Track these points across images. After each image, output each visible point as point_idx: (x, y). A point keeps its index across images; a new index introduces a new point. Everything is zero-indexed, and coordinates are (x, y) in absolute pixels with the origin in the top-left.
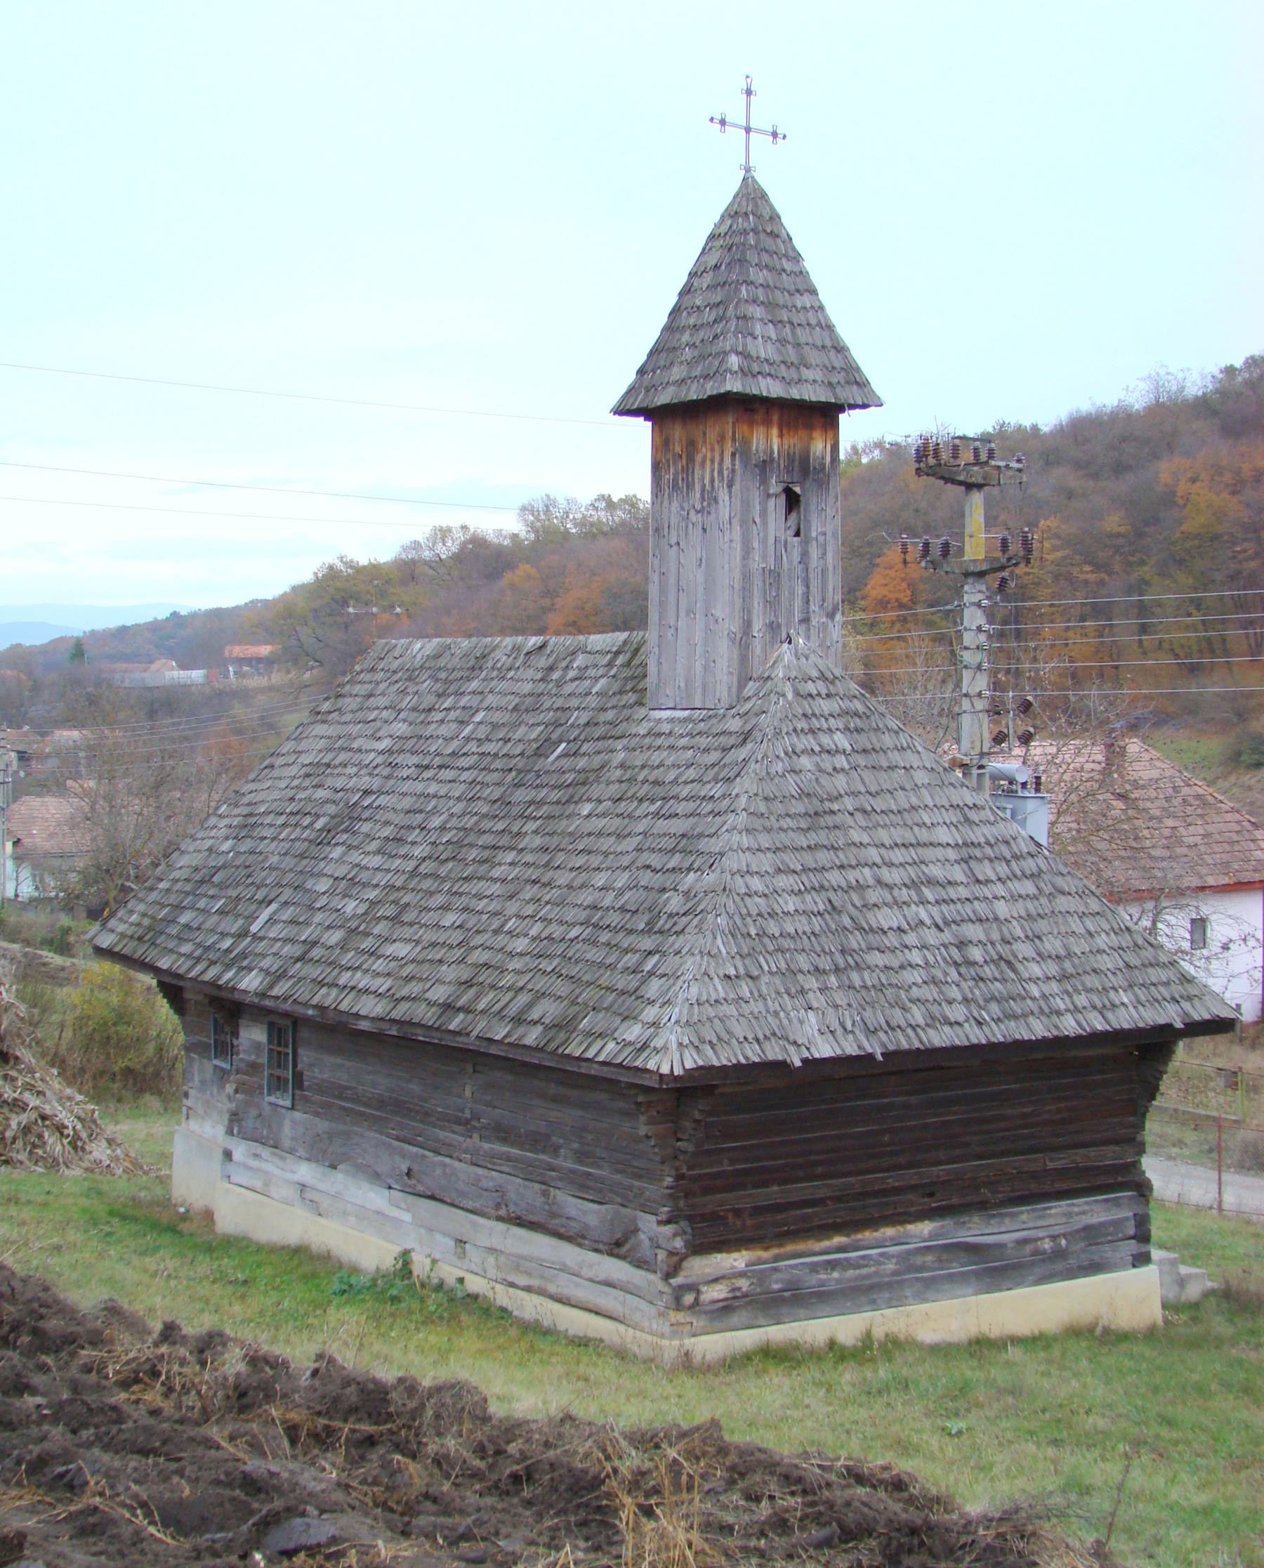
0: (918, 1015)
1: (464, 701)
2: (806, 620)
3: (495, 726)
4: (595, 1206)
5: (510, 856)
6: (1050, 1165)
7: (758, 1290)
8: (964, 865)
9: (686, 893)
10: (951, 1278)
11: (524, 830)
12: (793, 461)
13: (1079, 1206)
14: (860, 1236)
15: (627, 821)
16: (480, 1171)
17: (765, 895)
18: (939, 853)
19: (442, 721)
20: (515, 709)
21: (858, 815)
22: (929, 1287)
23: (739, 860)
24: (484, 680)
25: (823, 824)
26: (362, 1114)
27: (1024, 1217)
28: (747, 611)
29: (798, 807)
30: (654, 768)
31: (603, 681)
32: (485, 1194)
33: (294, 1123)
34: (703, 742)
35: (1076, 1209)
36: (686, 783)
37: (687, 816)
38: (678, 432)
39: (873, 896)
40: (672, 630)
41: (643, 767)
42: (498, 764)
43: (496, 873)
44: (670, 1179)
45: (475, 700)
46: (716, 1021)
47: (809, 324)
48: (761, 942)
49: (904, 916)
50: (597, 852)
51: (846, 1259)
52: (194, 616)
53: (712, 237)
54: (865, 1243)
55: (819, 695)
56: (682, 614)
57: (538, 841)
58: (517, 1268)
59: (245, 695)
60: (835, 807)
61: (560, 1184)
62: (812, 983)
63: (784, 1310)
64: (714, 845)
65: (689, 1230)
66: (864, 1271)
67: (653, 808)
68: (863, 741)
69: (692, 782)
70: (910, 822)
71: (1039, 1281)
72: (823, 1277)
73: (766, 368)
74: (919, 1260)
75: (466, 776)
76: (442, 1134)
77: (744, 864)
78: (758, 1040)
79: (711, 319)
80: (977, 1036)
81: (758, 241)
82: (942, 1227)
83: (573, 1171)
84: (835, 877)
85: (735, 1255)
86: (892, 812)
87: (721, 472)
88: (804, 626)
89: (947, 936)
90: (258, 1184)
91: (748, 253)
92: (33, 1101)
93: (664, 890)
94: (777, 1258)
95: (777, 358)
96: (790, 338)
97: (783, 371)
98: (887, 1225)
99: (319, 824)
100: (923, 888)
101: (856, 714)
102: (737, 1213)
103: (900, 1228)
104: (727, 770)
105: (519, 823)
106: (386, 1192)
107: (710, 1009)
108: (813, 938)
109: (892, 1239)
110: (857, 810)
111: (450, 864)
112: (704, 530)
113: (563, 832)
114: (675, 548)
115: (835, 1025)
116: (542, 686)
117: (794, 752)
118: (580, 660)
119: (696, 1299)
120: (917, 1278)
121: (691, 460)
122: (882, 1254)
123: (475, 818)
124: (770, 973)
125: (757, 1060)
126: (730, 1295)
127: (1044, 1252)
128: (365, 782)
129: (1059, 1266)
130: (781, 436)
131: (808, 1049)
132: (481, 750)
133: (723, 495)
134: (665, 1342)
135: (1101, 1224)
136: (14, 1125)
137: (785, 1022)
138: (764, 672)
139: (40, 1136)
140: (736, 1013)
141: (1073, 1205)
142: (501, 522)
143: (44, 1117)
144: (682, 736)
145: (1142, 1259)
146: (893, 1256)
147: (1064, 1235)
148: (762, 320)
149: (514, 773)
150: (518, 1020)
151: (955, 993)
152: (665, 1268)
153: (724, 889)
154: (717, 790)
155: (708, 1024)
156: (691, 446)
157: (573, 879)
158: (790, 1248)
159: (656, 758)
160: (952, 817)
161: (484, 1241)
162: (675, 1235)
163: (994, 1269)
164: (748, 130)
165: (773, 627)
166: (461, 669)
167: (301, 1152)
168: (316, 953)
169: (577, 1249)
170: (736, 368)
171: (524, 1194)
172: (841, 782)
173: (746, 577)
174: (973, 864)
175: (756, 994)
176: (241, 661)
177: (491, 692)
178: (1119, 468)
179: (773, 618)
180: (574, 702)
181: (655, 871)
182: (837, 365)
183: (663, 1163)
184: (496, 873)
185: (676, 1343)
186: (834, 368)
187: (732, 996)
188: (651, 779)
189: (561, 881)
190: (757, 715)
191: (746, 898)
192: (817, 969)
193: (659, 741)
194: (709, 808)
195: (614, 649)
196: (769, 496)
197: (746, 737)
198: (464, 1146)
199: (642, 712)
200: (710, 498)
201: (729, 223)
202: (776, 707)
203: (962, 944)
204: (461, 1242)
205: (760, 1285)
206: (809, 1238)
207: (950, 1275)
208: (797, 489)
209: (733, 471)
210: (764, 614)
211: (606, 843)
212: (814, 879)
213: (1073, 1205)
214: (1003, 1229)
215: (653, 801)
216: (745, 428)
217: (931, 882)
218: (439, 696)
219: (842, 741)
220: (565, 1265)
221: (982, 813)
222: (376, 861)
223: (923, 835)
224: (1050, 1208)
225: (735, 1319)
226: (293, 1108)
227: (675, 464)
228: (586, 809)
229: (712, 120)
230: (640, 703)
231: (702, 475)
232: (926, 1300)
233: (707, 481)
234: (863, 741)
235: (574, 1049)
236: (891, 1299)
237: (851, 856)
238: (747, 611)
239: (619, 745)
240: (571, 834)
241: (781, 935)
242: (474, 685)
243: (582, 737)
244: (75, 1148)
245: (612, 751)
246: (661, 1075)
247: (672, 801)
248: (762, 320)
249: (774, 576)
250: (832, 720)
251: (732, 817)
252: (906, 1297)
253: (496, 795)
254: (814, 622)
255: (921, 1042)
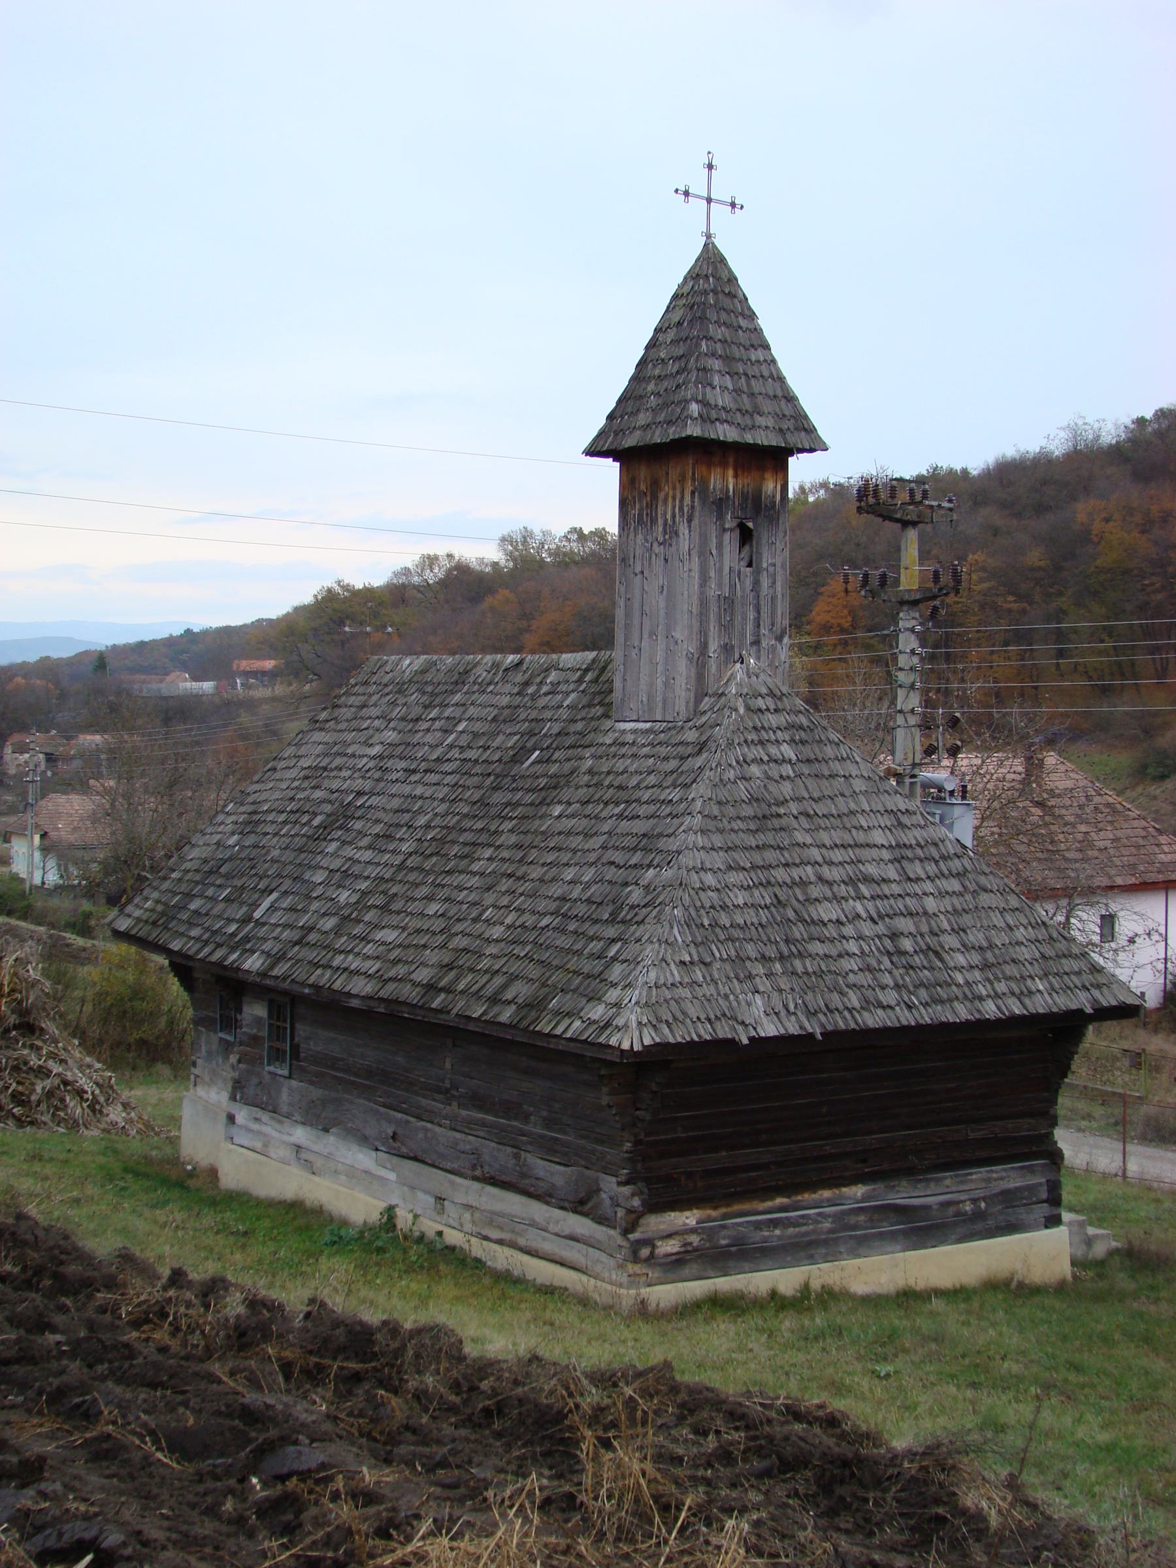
0: (854, 1000)
1: (448, 712)
2: (756, 643)
3: (476, 735)
4: (562, 1168)
5: (488, 852)
6: (972, 1136)
7: (708, 1245)
8: (897, 865)
9: (647, 887)
10: (881, 1236)
11: (500, 829)
12: (747, 499)
13: (996, 1172)
14: (799, 1198)
15: (593, 821)
16: (458, 1135)
17: (718, 890)
18: (875, 853)
19: (428, 730)
20: (494, 719)
21: (802, 819)
22: (862, 1244)
23: (694, 858)
24: (466, 693)
25: (770, 826)
26: (353, 1083)
27: (948, 1182)
28: (703, 633)
29: (748, 811)
30: (618, 774)
31: (573, 696)
32: (463, 1156)
33: (290, 1091)
34: (663, 751)
35: (995, 1175)
36: (647, 788)
37: (648, 818)
38: (643, 473)
39: (815, 891)
40: (636, 651)
41: (609, 773)
42: (478, 769)
43: (475, 867)
44: (629, 1144)
45: (458, 712)
46: (672, 1003)
47: (762, 376)
48: (714, 932)
49: (843, 910)
50: (567, 849)
51: (786, 1218)
52: (206, 633)
53: (676, 297)
54: (804, 1204)
55: (768, 710)
56: (645, 636)
57: (513, 839)
58: (490, 1223)
59: (250, 705)
60: (782, 811)
61: (530, 1148)
62: (758, 969)
63: (731, 1264)
64: (673, 844)
65: (646, 1190)
66: (804, 1229)
67: (617, 810)
68: (807, 752)
69: (653, 787)
70: (848, 825)
71: (960, 1240)
72: (766, 1234)
73: (724, 415)
74: (853, 1220)
75: (449, 779)
76: (424, 1102)
77: (699, 861)
78: (709, 1020)
79: (674, 370)
80: (906, 1018)
81: (717, 301)
82: (874, 1190)
83: (542, 1136)
84: (780, 874)
85: (687, 1213)
86: (833, 816)
87: (681, 509)
88: (755, 648)
89: (881, 928)
90: (258, 1145)
91: (708, 314)
92: (56, 1069)
93: (626, 884)
94: (725, 1217)
95: (733, 406)
96: (745, 389)
97: (739, 418)
98: (824, 1188)
99: (316, 822)
100: (860, 885)
101: (801, 727)
102: (690, 1175)
103: (837, 1191)
104: (684, 776)
105: (496, 823)
106: (373, 1154)
107: (667, 992)
108: (760, 929)
109: (828, 1200)
110: (801, 813)
111: (434, 859)
112: (666, 560)
113: (536, 831)
114: (639, 576)
115: (779, 1007)
116: (518, 699)
117: (745, 761)
118: (553, 677)
119: (652, 1253)
120: (851, 1237)
121: (655, 497)
122: (819, 1214)
123: (457, 817)
124: (721, 959)
125: (708, 1038)
126: (682, 1249)
127: (965, 1214)
128: (359, 784)
129: (979, 1226)
130: (736, 476)
131: (755, 1029)
132: (463, 756)
133: (683, 529)
134: (623, 1291)
135: (1016, 1188)
136: (39, 1089)
137: (735, 1004)
138: (718, 689)
139: (62, 1100)
140: (690, 996)
141: (992, 1171)
142: (483, 551)
143: (66, 1083)
144: (644, 745)
145: (1053, 1221)
146: (829, 1216)
147: (984, 1199)
148: (720, 372)
149: (492, 778)
150: (494, 1000)
151: (887, 979)
152: (624, 1224)
153: (681, 884)
154: (675, 795)
155: (665, 1005)
156: (655, 485)
157: (545, 873)
158: (736, 1208)
159: (620, 765)
160: (886, 821)
161: (461, 1198)
162: (633, 1195)
163: (919, 1228)
164: (709, 200)
165: (727, 649)
166: (446, 683)
167: (297, 1117)
168: (312, 937)
169: (545, 1207)
170: (696, 414)
171: (498, 1156)
172: (787, 789)
173: (703, 602)
174: (905, 863)
175: (708, 979)
176: (247, 674)
177: (472, 704)
178: (1041, 509)
179: (727, 640)
180: (548, 714)
181: (619, 867)
182: (787, 413)
183: (623, 1130)
184: (475, 867)
185: (633, 1292)
186: (784, 416)
187: (687, 980)
188: (616, 784)
189: (534, 875)
190: (711, 727)
191: (701, 892)
192: (763, 957)
193: (623, 750)
194: (668, 810)
195: (584, 667)
196: (724, 530)
197: (702, 747)
198: (444, 1112)
199: (608, 724)
200: (672, 532)
201: (691, 284)
202: (729, 720)
203: (894, 936)
204: (440, 1199)
205: (709, 1241)
206: (754, 1198)
207: (881, 1233)
208: (750, 525)
209: (693, 507)
210: (719, 637)
211: (575, 842)
212: (762, 876)
213: (992, 1171)
214: (929, 1193)
215: (617, 804)
216: (704, 468)
217: (868, 879)
218: (426, 707)
219: (788, 751)
220: (533, 1220)
221: (914, 817)
222: (368, 855)
223: (861, 837)
224: (971, 1174)
225: (686, 1271)
226: (290, 1077)
227: (640, 501)
228: (557, 810)
229: (676, 191)
230: (606, 716)
231: (666, 511)
232: (859, 1256)
233: (669, 517)
234: (807, 752)
235: (544, 1027)
236: (827, 1254)
237: (795, 855)
238: (703, 633)
239: (587, 753)
240: (543, 833)
241: (732, 926)
242: (457, 697)
243: (554, 746)
244: (94, 1111)
245: (581, 759)
246: (622, 1051)
247: (634, 804)
248: (720, 372)
249: (728, 603)
250: (779, 733)
251: (688, 820)
252: (841, 1253)
253: (476, 797)
254: (764, 644)
255: (857, 1023)
